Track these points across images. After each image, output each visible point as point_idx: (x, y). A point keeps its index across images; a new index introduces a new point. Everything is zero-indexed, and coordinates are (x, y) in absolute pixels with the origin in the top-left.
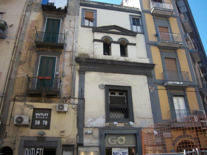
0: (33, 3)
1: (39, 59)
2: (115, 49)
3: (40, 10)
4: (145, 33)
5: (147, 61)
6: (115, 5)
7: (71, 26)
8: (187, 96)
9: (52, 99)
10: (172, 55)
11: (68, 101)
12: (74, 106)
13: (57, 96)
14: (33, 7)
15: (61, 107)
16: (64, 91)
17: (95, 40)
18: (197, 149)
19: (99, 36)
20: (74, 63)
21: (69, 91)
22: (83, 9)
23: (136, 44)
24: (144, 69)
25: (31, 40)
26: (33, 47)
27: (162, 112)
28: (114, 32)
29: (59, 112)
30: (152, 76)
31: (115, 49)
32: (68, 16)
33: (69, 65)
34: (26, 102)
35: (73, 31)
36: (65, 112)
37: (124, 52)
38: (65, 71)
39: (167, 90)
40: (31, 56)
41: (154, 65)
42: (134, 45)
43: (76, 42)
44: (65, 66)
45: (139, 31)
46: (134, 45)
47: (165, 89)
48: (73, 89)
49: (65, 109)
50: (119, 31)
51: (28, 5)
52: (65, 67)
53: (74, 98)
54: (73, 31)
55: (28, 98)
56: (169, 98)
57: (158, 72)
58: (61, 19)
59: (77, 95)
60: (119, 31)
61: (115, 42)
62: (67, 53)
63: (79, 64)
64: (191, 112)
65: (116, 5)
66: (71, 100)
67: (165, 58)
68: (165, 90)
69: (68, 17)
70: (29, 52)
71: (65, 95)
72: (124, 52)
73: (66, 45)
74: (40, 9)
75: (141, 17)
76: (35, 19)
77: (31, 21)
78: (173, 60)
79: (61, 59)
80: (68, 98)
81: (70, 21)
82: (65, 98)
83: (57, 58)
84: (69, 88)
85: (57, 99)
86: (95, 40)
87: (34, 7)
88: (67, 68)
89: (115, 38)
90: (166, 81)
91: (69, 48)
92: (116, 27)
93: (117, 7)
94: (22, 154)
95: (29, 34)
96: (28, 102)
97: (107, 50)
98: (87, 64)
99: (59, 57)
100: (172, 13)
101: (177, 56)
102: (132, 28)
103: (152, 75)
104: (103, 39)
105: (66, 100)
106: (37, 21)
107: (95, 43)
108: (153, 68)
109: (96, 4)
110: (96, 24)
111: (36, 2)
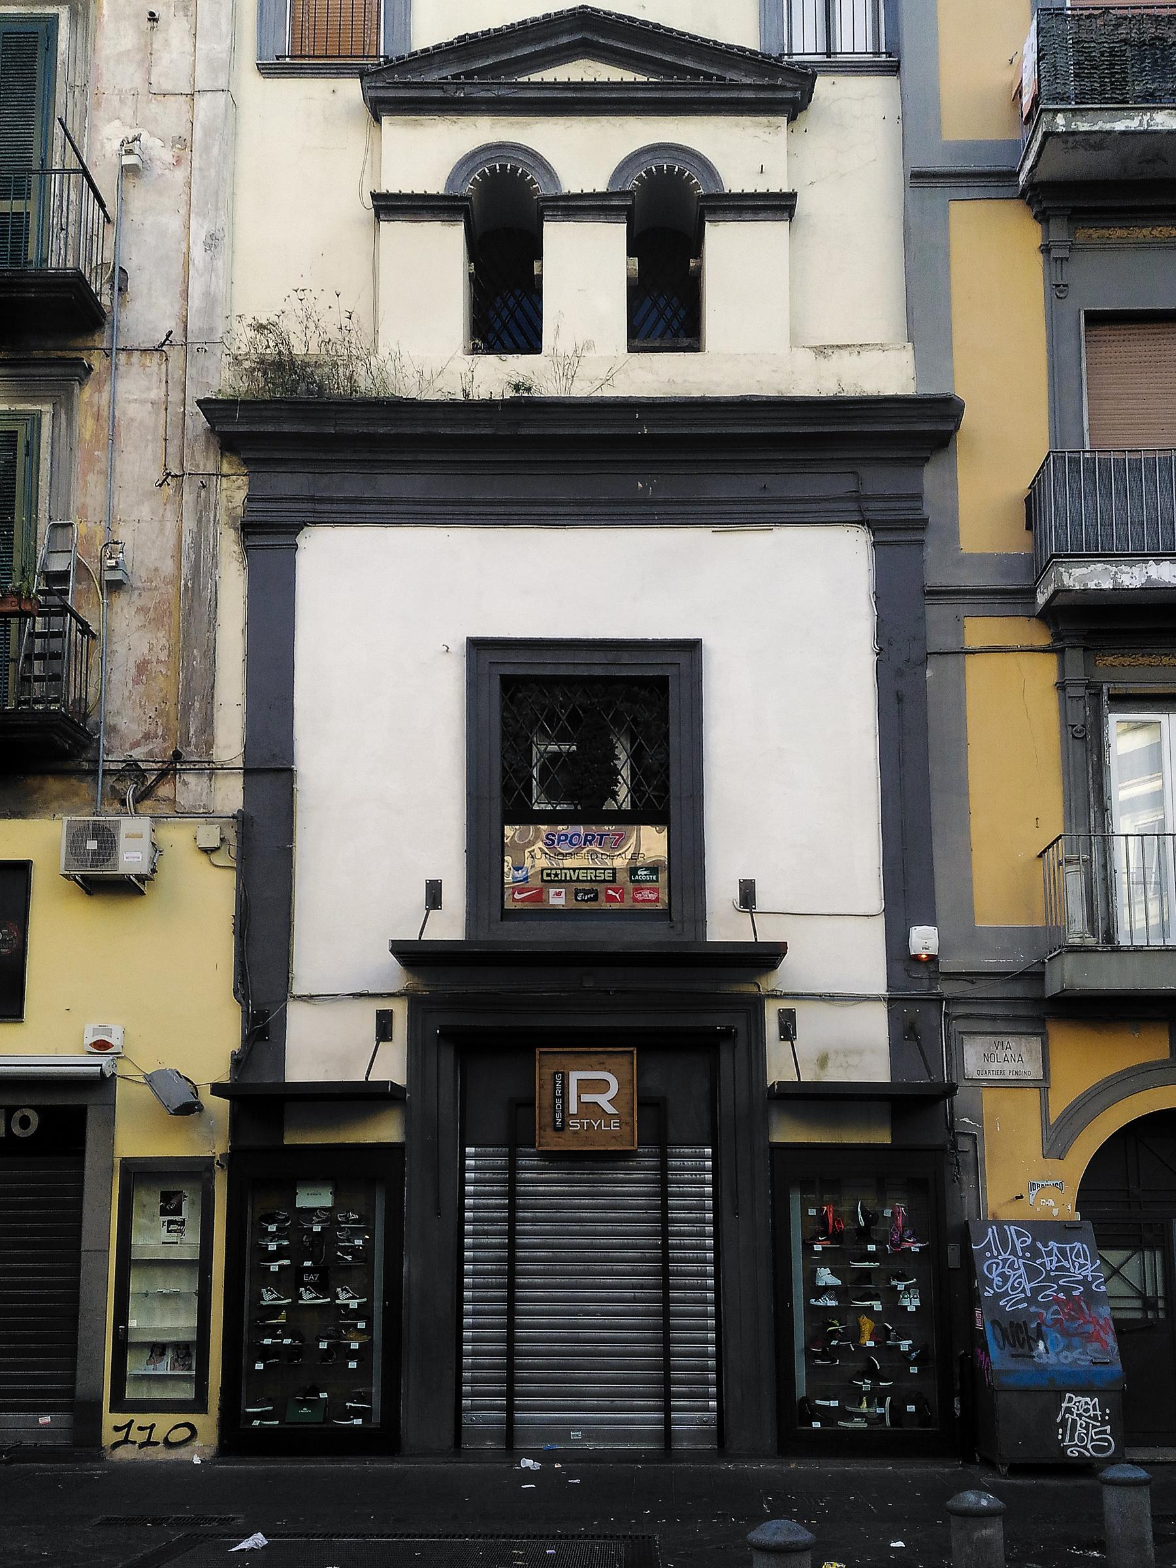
2: (585, 273)
5: (888, 374)
7: (161, 81)
11: (164, 790)
15: (92, 845)
16: (128, 718)
17: (390, 206)
19: (429, 151)
20: (204, 460)
21: (169, 707)
23: (793, 196)
28: (581, 86)
31: (585, 273)
33: (158, 476)
35: (183, 131)
37: (666, 306)
38: (123, 534)
39: (1060, 652)
42: (779, 206)
43: (212, 243)
46: (779, 206)
48: (197, 693)
49: (131, 859)
50: (629, 76)
52: (122, 502)
56: (1066, 725)
57: (983, 494)
58: (63, 13)
59: (229, 739)
60: (629, 76)
61: (579, 207)
62: (135, 369)
63: (246, 462)
66: (185, 784)
68: (1043, 650)
72: (666, 306)
73: (120, 281)
79: (86, 426)
80: (163, 775)
81: (152, 17)
82: (133, 769)
83: (46, 421)
84: (163, 682)
86: (390, 206)
88: (145, 511)
89: (583, 153)
91: (146, 313)
97: (505, 309)
98: (312, 446)
103: (928, 511)
104: (467, 189)
105: (143, 784)
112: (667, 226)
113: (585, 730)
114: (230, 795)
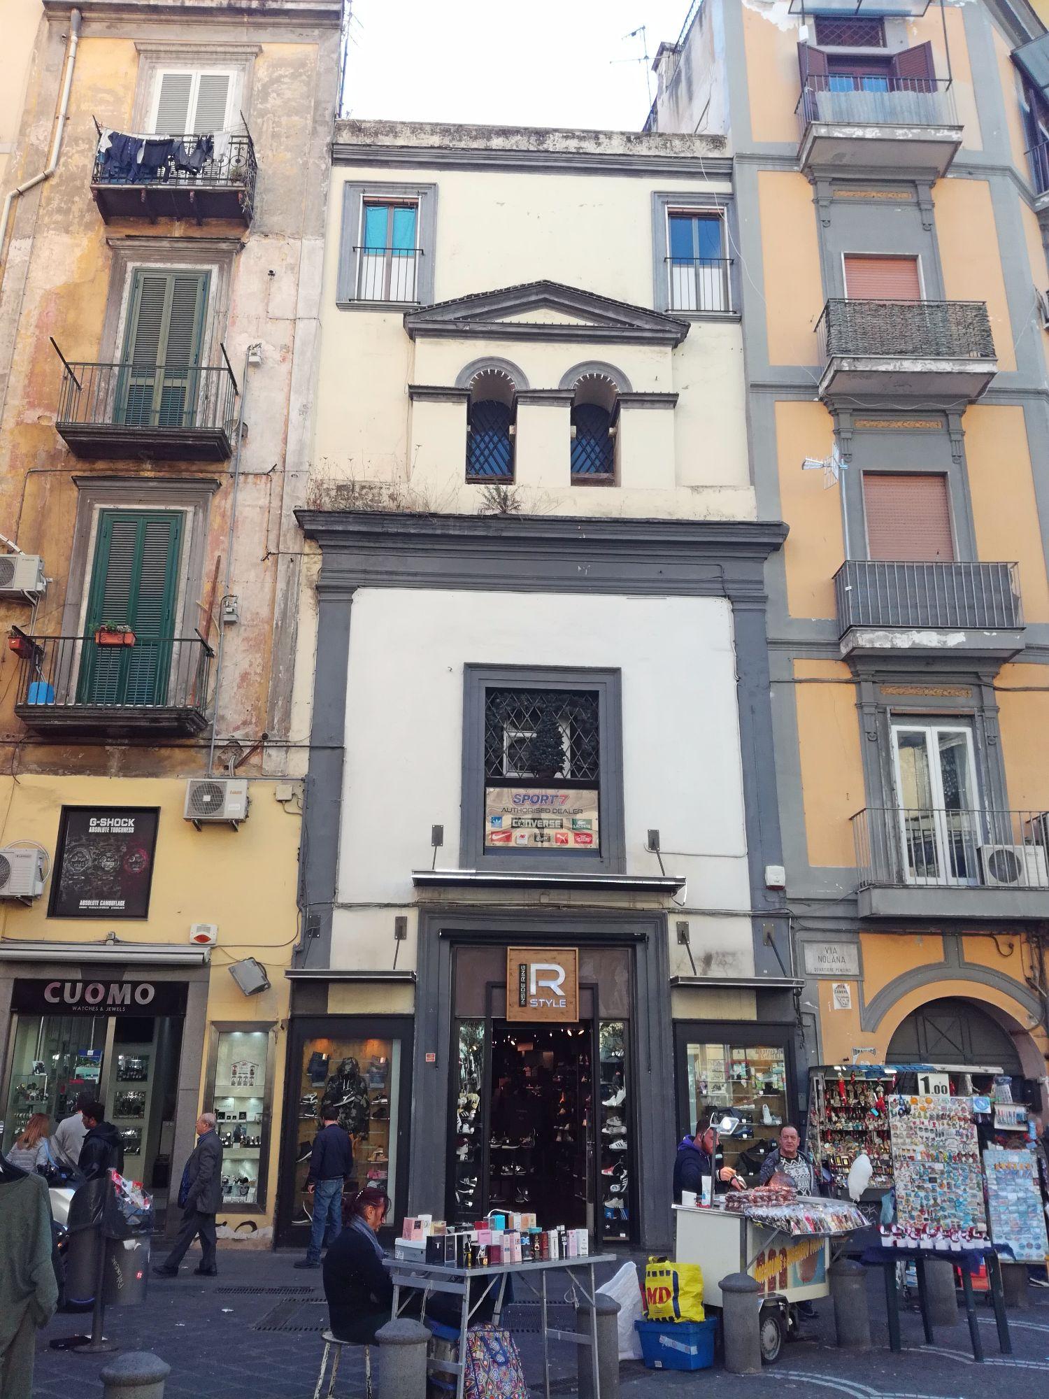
0: (46, 178)
1: (88, 533)
2: (543, 437)
3: (88, 217)
4: (746, 319)
5: (738, 505)
6: (556, 130)
7: (275, 310)
8: (995, 718)
9: (165, 752)
10: (932, 456)
11: (254, 760)
12: (285, 791)
13: (191, 735)
14: (49, 200)
15: (207, 798)
16: (231, 711)
17: (418, 393)
18: (837, 1006)
19: (447, 361)
20: (293, 542)
22: (350, 184)
24: (716, 555)
25: (39, 412)
26: (53, 457)
27: (809, 817)
29: (199, 825)
30: (764, 599)
31: (543, 437)
32: (253, 242)
34: (21, 773)
36: (232, 826)
37: (595, 454)
40: (43, 514)
41: (779, 529)
43: (305, 410)
44: (241, 549)
45: (713, 300)
47: (848, 676)
48: (281, 694)
49: (232, 808)
51: (21, 194)
53: (287, 747)
54: (288, 341)
55: (34, 754)
57: (804, 581)
58: (215, 269)
59: (301, 729)
61: (539, 397)
62: (250, 485)
64: (1016, 821)
65: (569, 134)
66: (270, 756)
67: (867, 473)
68: (847, 682)
69: (257, 252)
70: (30, 487)
71: (237, 728)
72: (595, 454)
74: (88, 210)
75: (732, 196)
76: (59, 279)
77: (41, 292)
78: (937, 482)
79: (216, 521)
80: (254, 748)
81: (271, 273)
82: (234, 745)
83: (190, 516)
85: (193, 752)
86: (418, 393)
87: (55, 204)
88: (252, 575)
89: (544, 366)
90: (845, 631)
91: (257, 452)
92: (548, 293)
93: (572, 145)
94: (697, 275)
95: (31, 375)
96: (31, 772)
98: (363, 538)
99: (203, 505)
100: (949, 149)
101: (959, 458)
102: (661, 284)
103: (767, 591)
105: (241, 755)
106: (70, 295)
107: (421, 406)
108: (776, 547)
109: (435, 140)
110: (425, 276)
111: (66, 164)
112: (596, 417)
113: (544, 729)
114: (299, 764)
